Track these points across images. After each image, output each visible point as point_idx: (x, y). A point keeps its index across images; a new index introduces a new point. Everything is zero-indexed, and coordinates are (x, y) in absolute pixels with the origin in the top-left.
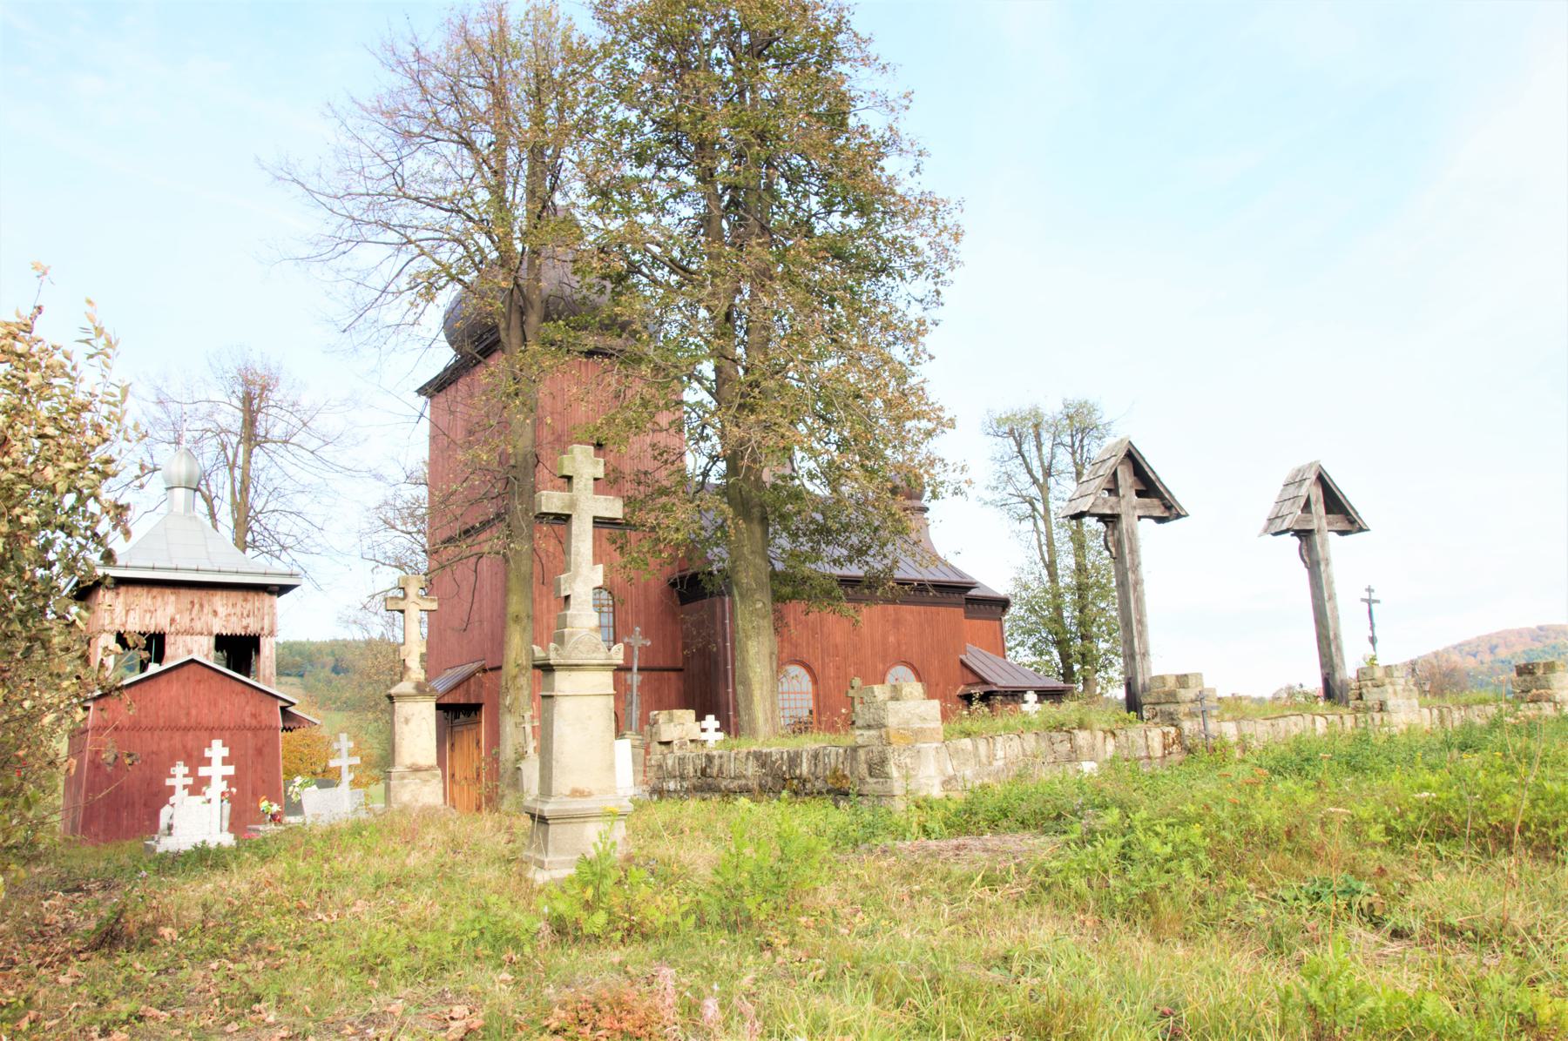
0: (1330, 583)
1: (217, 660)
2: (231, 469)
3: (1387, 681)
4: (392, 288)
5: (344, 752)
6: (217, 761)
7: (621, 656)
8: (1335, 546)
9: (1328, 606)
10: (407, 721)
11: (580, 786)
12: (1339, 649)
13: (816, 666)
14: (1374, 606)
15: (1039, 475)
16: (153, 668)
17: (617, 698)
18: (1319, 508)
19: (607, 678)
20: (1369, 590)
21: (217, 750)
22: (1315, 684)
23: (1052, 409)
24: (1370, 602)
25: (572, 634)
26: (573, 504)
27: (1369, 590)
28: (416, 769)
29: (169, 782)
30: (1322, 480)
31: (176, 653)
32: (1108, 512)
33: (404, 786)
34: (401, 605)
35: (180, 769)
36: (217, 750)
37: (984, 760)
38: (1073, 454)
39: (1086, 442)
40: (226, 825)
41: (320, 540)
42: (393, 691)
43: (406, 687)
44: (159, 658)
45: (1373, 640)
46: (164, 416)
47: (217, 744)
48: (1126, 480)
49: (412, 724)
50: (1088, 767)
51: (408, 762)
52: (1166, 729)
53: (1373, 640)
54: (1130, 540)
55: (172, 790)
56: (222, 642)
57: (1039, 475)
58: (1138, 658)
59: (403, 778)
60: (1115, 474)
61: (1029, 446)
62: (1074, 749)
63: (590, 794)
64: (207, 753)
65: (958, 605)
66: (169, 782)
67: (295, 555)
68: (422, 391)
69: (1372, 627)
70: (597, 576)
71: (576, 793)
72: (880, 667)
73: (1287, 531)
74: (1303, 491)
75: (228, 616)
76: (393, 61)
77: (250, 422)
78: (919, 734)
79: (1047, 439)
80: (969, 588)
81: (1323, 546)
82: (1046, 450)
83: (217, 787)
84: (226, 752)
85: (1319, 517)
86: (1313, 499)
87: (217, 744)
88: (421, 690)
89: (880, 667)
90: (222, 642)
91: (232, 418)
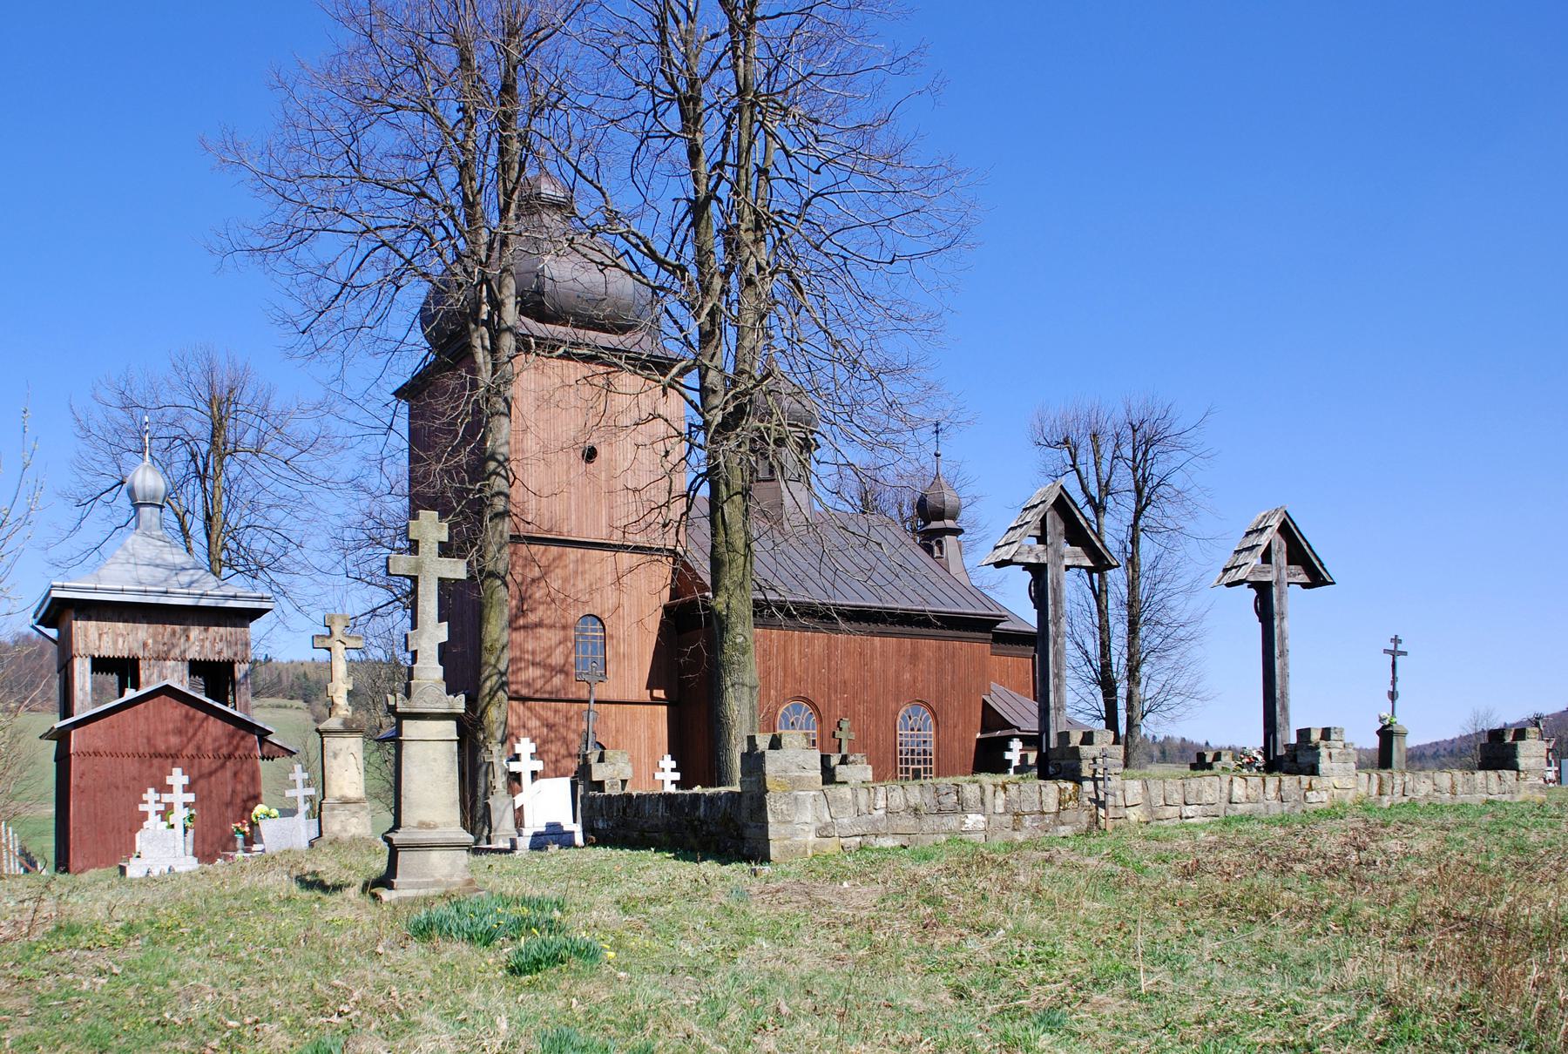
0: (1283, 639)
1: (192, 687)
2: (203, 482)
3: (1323, 743)
4: (356, 281)
5: (299, 784)
6: (178, 789)
7: (463, 705)
8: (1295, 601)
9: (1277, 663)
10: (335, 756)
11: (426, 819)
12: (1284, 708)
13: (820, 703)
14: (1399, 659)
15: (1094, 490)
16: (130, 694)
17: (460, 743)
18: (1279, 557)
19: (451, 726)
20: (1396, 640)
21: (178, 778)
22: (1253, 741)
23: (1114, 417)
24: (1394, 654)
25: (418, 685)
26: (419, 567)
27: (1396, 640)
28: (345, 802)
29: (142, 808)
30: (1286, 530)
31: (151, 679)
32: (1033, 561)
33: (333, 817)
34: (328, 643)
35: (151, 795)
36: (178, 778)
37: (863, 809)
38: (1135, 470)
39: (1150, 454)
40: (190, 849)
41: (299, 558)
42: (321, 727)
43: (333, 723)
44: (136, 686)
45: (1393, 696)
46: (129, 422)
47: (177, 771)
48: (1056, 526)
49: (340, 759)
50: (974, 820)
51: (337, 795)
52: (1063, 784)
53: (1393, 696)
54: (1054, 590)
55: (145, 816)
56: (196, 667)
57: (1094, 490)
58: (1052, 712)
59: (333, 809)
60: (1043, 520)
61: (1085, 458)
62: (960, 801)
63: (435, 827)
64: (169, 780)
65: (985, 641)
66: (142, 808)
67: (273, 575)
68: (398, 394)
69: (1394, 683)
70: (442, 633)
71: (423, 825)
72: (892, 706)
73: (1240, 582)
74: (1264, 540)
75: (203, 643)
76: (344, 13)
77: (217, 429)
78: (797, 783)
79: (1107, 452)
80: (998, 622)
81: (1280, 599)
82: (1105, 467)
83: (180, 815)
84: (185, 780)
85: (1281, 571)
86: (1275, 547)
87: (177, 771)
88: (348, 729)
89: (892, 706)
90: (196, 667)
91: (197, 426)
